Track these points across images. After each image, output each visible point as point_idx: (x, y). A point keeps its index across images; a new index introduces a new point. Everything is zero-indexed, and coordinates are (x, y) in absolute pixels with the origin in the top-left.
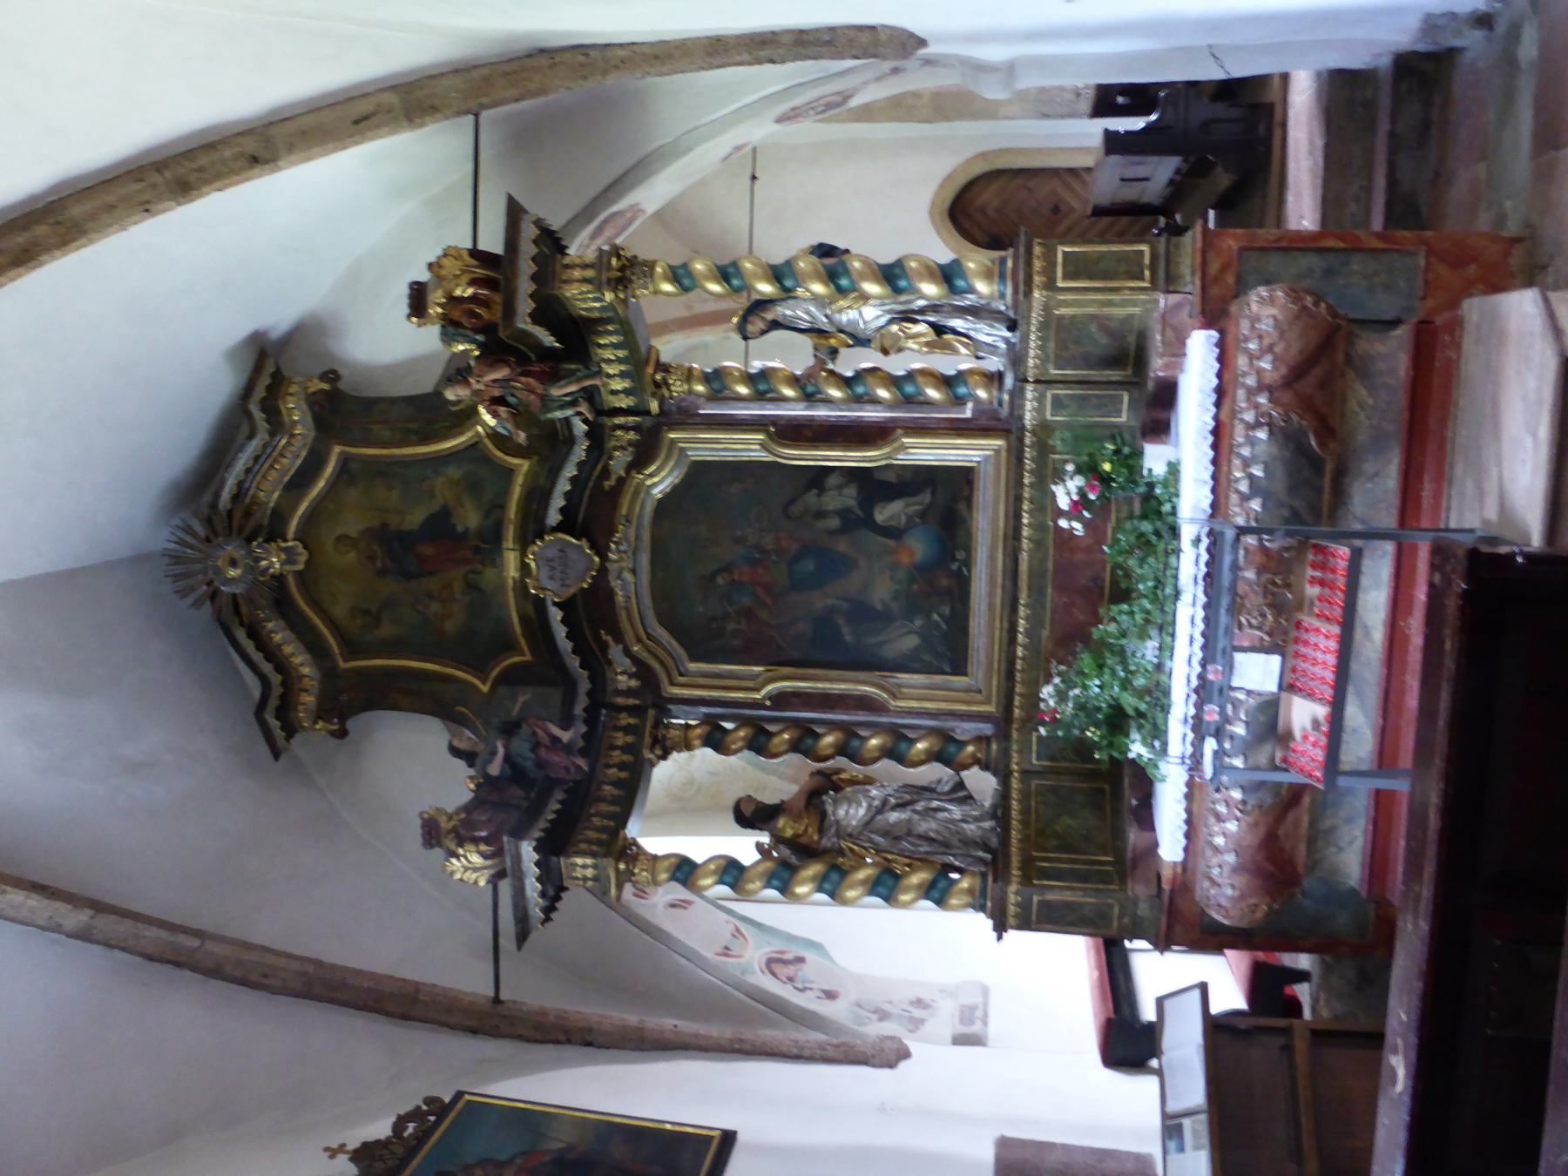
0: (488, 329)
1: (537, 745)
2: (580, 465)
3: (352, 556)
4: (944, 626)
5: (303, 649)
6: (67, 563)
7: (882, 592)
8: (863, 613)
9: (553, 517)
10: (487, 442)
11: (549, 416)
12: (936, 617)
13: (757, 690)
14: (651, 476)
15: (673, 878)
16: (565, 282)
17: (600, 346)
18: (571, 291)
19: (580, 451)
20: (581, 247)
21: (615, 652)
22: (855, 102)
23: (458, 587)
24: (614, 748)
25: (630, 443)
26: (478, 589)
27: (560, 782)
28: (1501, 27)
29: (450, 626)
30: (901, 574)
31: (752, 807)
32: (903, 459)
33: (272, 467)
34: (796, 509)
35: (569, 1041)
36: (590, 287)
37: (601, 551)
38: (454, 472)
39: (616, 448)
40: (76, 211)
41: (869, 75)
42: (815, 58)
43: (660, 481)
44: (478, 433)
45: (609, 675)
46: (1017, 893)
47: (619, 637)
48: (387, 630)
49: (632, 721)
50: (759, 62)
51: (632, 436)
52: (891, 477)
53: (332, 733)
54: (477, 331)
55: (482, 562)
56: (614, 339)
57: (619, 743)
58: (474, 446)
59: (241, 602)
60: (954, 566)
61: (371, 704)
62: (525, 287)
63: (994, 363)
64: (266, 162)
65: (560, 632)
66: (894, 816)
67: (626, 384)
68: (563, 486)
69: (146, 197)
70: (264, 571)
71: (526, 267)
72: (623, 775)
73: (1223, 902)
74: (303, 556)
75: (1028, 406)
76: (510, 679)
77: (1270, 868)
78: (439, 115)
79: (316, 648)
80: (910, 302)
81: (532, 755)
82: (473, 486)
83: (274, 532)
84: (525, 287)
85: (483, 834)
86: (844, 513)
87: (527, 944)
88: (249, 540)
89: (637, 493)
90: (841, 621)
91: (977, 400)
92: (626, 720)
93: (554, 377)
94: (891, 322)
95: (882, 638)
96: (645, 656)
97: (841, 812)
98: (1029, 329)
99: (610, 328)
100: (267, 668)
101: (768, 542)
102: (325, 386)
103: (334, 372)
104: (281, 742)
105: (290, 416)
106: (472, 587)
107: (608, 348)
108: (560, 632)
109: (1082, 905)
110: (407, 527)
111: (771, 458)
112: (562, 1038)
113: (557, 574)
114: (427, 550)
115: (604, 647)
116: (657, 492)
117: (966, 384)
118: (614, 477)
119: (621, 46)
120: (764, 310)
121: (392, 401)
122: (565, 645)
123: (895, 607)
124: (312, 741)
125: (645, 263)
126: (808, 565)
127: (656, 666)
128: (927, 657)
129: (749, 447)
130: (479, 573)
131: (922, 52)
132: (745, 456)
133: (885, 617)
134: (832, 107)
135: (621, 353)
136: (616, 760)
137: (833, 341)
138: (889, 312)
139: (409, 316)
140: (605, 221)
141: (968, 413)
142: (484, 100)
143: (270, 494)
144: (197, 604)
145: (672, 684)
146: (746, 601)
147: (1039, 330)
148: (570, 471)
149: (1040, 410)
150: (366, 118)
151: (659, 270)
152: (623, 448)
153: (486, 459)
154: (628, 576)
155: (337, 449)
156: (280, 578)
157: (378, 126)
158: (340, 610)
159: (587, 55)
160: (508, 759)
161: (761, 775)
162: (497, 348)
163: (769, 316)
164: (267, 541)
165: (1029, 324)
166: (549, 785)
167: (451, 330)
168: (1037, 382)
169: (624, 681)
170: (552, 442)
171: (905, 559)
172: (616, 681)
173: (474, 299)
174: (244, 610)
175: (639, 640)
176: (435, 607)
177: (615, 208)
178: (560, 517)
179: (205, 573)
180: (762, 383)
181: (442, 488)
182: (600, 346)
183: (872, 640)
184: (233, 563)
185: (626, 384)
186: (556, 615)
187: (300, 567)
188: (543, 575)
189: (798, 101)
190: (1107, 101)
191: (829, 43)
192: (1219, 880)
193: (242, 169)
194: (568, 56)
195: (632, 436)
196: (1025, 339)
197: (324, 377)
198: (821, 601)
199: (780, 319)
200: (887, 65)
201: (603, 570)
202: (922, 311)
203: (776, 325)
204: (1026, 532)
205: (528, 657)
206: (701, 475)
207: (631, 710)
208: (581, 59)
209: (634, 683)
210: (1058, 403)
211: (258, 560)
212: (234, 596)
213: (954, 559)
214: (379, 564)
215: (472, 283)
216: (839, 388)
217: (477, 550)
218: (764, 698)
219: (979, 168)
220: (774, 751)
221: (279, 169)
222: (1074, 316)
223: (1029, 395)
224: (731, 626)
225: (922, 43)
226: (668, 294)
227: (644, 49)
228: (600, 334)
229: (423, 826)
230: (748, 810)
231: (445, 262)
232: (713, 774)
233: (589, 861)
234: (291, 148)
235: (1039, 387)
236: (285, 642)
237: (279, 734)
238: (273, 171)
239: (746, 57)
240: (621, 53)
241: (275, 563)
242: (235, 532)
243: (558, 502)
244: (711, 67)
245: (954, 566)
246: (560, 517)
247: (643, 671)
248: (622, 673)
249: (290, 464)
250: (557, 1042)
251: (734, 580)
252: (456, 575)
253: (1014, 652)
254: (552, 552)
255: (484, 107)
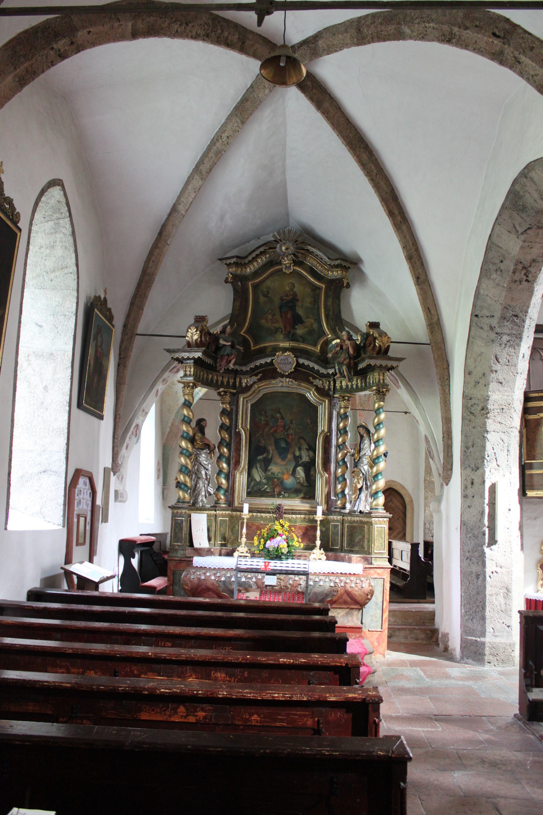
0: (365, 347)
1: (228, 355)
2: (318, 371)
3: (288, 289)
4: (263, 489)
5: (256, 269)
6: (289, 199)
7: (274, 469)
8: (267, 463)
9: (301, 361)
10: (326, 338)
11: (336, 365)
12: (266, 486)
13: (242, 427)
14: (314, 394)
15: (186, 400)
16: (379, 374)
17: (357, 380)
18: (376, 375)
19: (323, 371)
20: (389, 378)
21: (255, 379)
22: (431, 460)
23: (277, 325)
24: (223, 377)
25: (324, 387)
26: (276, 333)
27: (216, 362)
28: (446, 654)
29: (263, 321)
30: (280, 476)
31: (204, 425)
32: (318, 477)
33: (318, 262)
34: (302, 441)
35: (120, 358)
36: (377, 381)
37: (288, 376)
38: (315, 326)
39: (323, 382)
40: (404, 227)
41: (439, 467)
42: (444, 451)
43: (311, 396)
44: (328, 335)
45: (246, 376)
46: (185, 513)
47: (260, 380)
48: (262, 299)
49: (231, 384)
50: (443, 433)
51: (327, 387)
52: (312, 473)
53: (227, 278)
54: (365, 344)
55: (285, 334)
56: (359, 385)
57: (224, 380)
58: (324, 333)
59: (274, 250)
60: (283, 493)
61: (236, 291)
62: (378, 362)
63: (348, 506)
64: (417, 282)
65: (263, 361)
66: (203, 473)
67: (344, 387)
68: (312, 365)
69: (408, 247)
70: (282, 258)
71: (384, 363)
72: (215, 381)
73: (189, 575)
74: (288, 272)
75: (335, 517)
76: (245, 343)
77: (199, 590)
78: (430, 334)
79: (256, 274)
80: (369, 480)
81: (225, 354)
82: (311, 332)
83: (297, 263)
84: (378, 362)
85: (203, 339)
86: (300, 457)
87: (165, 351)
88: (294, 254)
89: (308, 388)
90: (264, 455)
91: (336, 501)
92: (231, 381)
93: (349, 367)
94: (363, 474)
95: (259, 469)
96: (253, 389)
97: (204, 455)
98: (360, 517)
99: (363, 384)
100: (250, 258)
101: (291, 431)
102: (345, 285)
103: (350, 286)
104: (225, 262)
105: (335, 271)
106: (277, 330)
107: (357, 382)
108: (263, 361)
109: (182, 533)
110: (297, 308)
111: (319, 434)
112: (122, 356)
113: (282, 362)
114: (289, 315)
115: (256, 375)
116: (308, 395)
117: (342, 497)
118: (313, 381)
119: (449, 390)
120: (367, 434)
121: (339, 306)
122: (258, 363)
123: (269, 473)
124: (225, 272)
125: (384, 399)
126: (283, 445)
127: (250, 393)
128: (252, 483)
129: (322, 427)
130: (282, 332)
131: (445, 484)
132: (319, 425)
133: (266, 470)
134: (429, 454)
135: (354, 386)
136: (219, 379)
137: (356, 455)
138: (366, 474)
139: (369, 322)
140: (395, 378)
141: (333, 498)
142: (434, 348)
143: (310, 261)
144: (274, 236)
145: (244, 398)
146: (271, 424)
147: (360, 520)
148: (316, 367)
149: (334, 521)
150: (430, 311)
151: (382, 403)
152: (323, 384)
153: (319, 337)
154: (280, 384)
155: (324, 286)
156: (280, 263)
157: (427, 316)
158: (268, 283)
159: (447, 380)
160: (224, 345)
161: (175, 412)
162: (359, 350)
163: (365, 435)
164: (293, 260)
165: (362, 517)
166: (215, 359)
167: (365, 336)
168: (343, 520)
169: (244, 381)
170: (324, 361)
171: (285, 477)
172: (245, 378)
173: (375, 345)
174: (271, 250)
175: (259, 387)
176: (270, 317)
177: (399, 382)
178: (301, 363)
179: (284, 239)
180: (343, 432)
181: (310, 321)
182: (357, 380)
183: (258, 466)
184: (287, 249)
185: (344, 387)
186: (269, 360)
187: (284, 270)
188: (282, 357)
189: (431, 443)
190: (429, 546)
191: (448, 455)
192: (195, 574)
193: (416, 275)
194: (446, 373)
195: (327, 387)
196: (357, 516)
197: (348, 284)
198: (271, 449)
199: (364, 438)
200: (441, 472)
201: (283, 376)
202: (366, 484)
203: (362, 437)
204: (294, 516)
205: (253, 348)
206: (315, 409)
207: (235, 383)
208: (446, 378)
209: (244, 384)
210: (336, 526)
211: (287, 256)
212: (276, 248)
213: (285, 493)
214: (285, 298)
215: (380, 346)
216: (341, 457)
217: (289, 332)
218: (239, 429)
219: (407, 500)
220: (222, 432)
221: (415, 286)
222: (364, 530)
223: (339, 517)
224: (263, 418)
225: (447, 484)
226: (374, 405)
227: (448, 398)
228: (361, 381)
229: (203, 316)
230: (203, 423)
231: (387, 337)
232: (176, 392)
233: (192, 373)
234: (421, 289)
235: (341, 521)
236: (258, 263)
237: (228, 262)
238: (415, 284)
239: (445, 429)
240: (447, 390)
241: (286, 261)
242: (297, 250)
243: (306, 363)
244: (442, 418)
245: (283, 493)
246: (301, 363)
247: (248, 388)
248: (247, 381)
249: (319, 269)
250: (120, 355)
251: (278, 419)
252: (281, 325)
253: (255, 512)
254: (290, 360)
255: (432, 347)
